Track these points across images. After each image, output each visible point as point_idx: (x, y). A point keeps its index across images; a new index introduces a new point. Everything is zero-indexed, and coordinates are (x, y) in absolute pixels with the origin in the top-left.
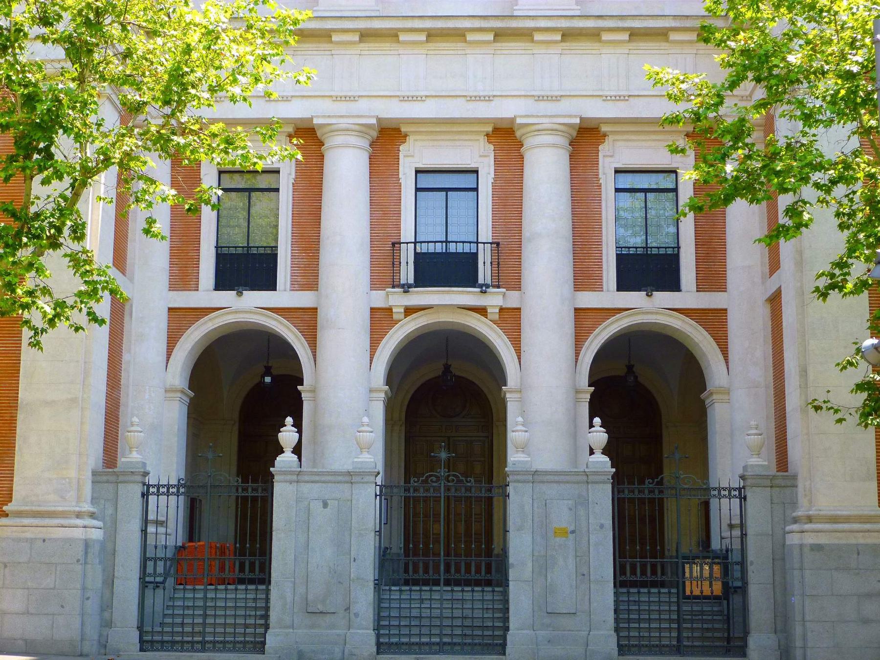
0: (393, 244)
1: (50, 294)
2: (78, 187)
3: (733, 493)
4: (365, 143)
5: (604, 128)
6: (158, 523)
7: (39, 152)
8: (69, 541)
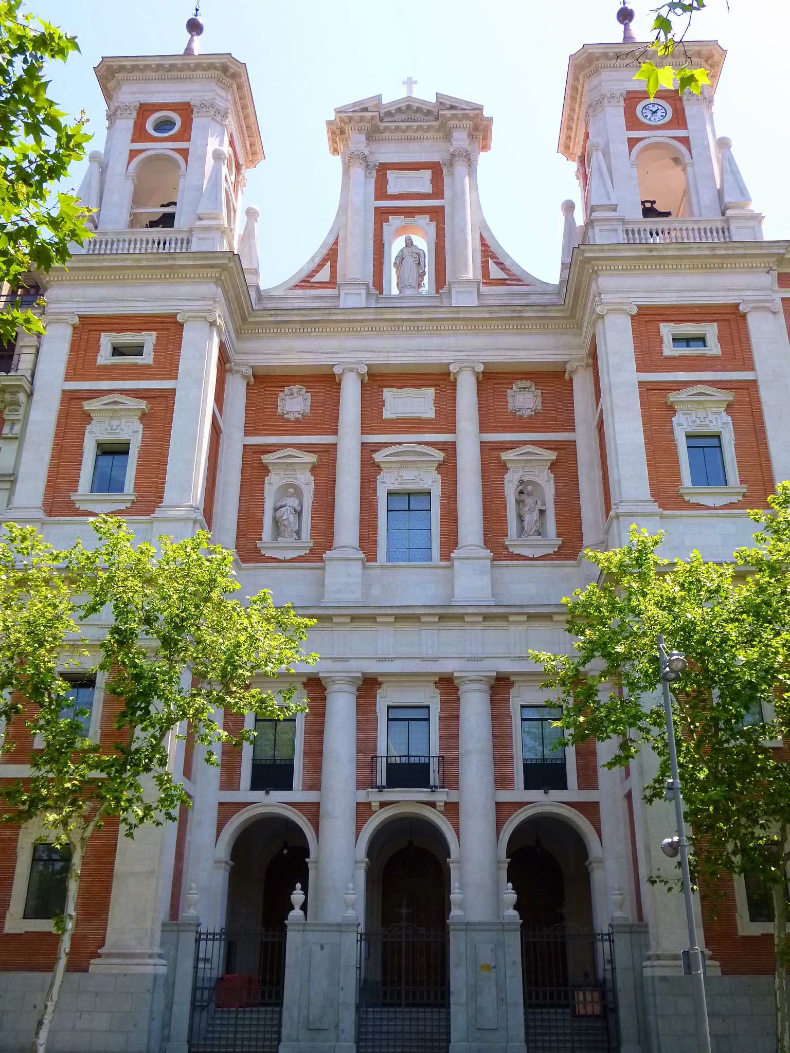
0: (372, 758)
1: (142, 801)
2: (164, 732)
3: (605, 937)
4: (354, 690)
5: (513, 678)
6: (206, 960)
7: (141, 709)
8: (143, 975)
